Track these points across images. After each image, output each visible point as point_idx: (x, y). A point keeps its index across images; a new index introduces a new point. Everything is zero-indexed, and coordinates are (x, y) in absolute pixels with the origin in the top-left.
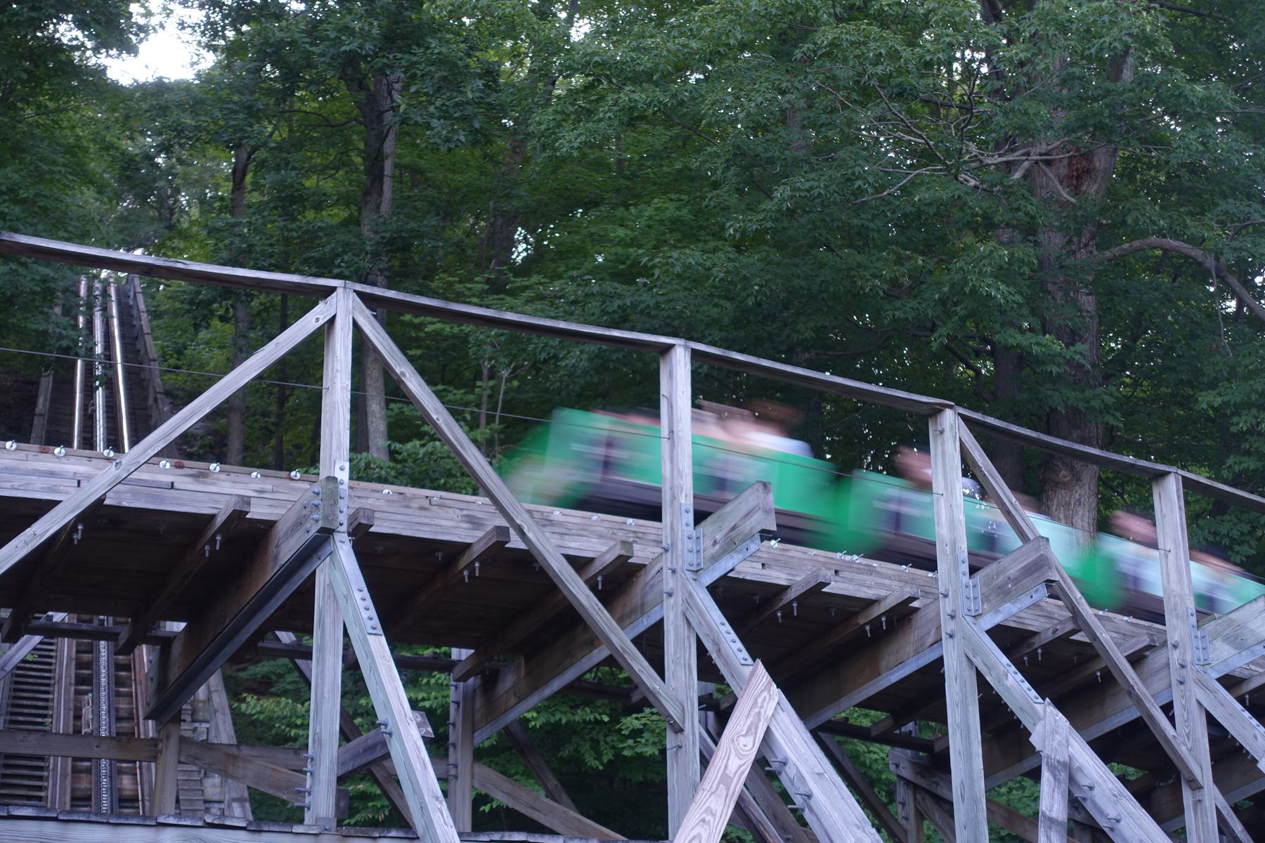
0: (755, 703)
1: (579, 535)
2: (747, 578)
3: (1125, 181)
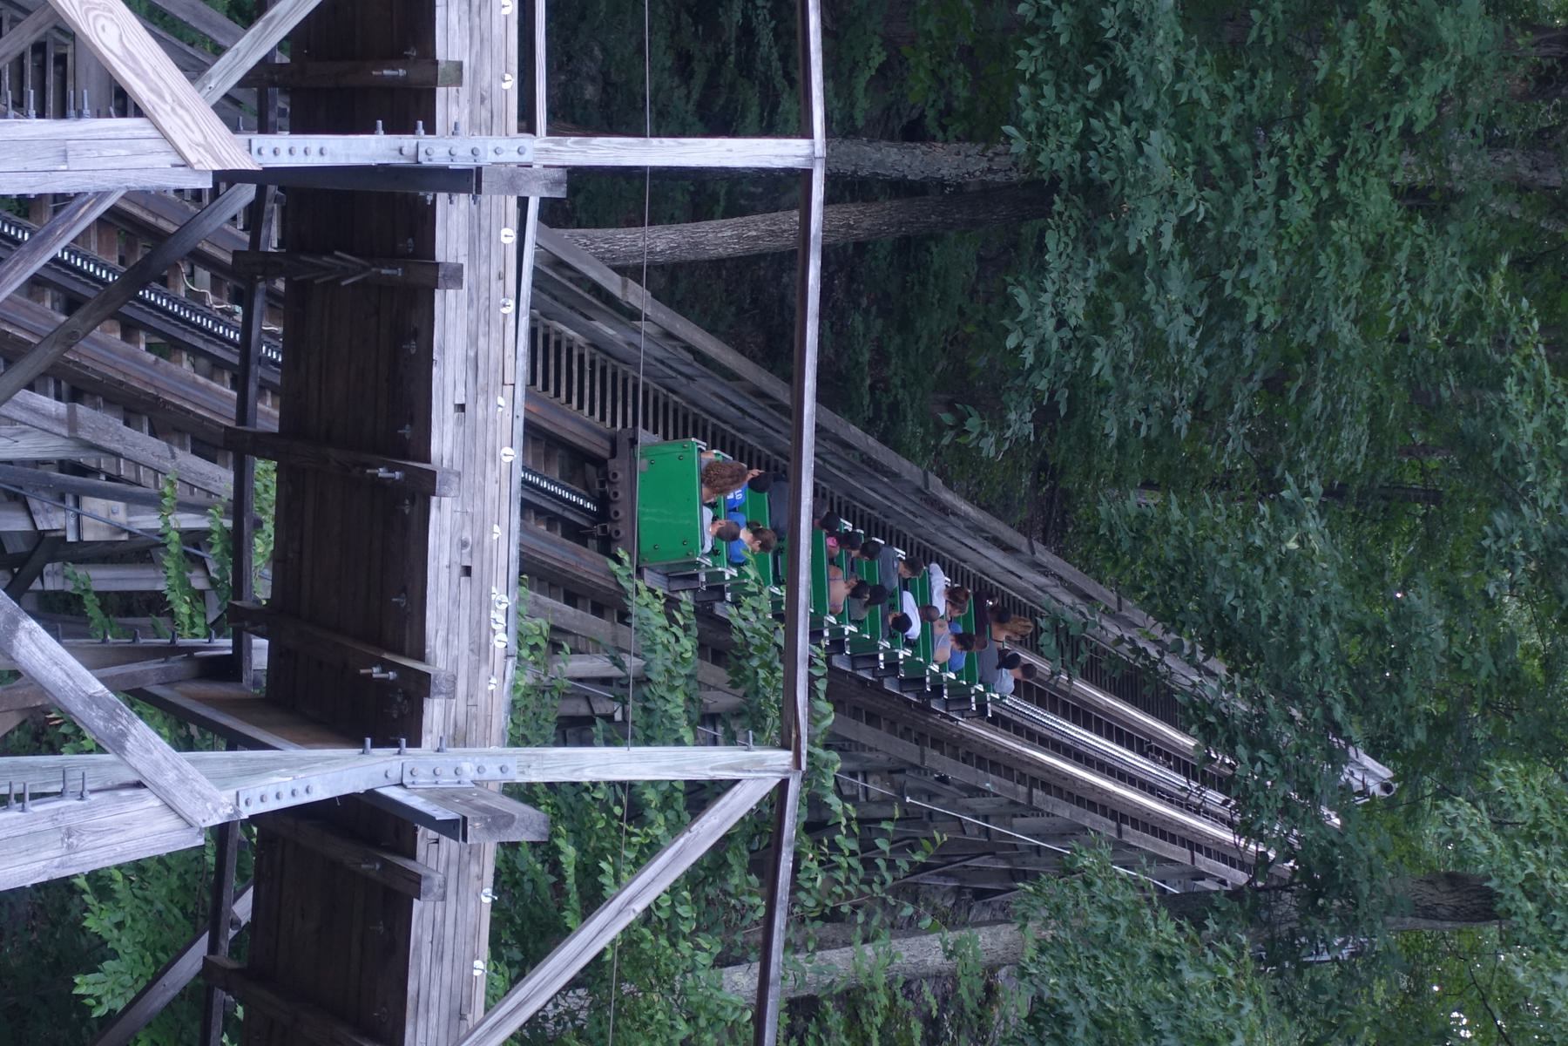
0: (181, 106)
1: (471, 29)
2: (435, 370)
3: (1364, 816)
